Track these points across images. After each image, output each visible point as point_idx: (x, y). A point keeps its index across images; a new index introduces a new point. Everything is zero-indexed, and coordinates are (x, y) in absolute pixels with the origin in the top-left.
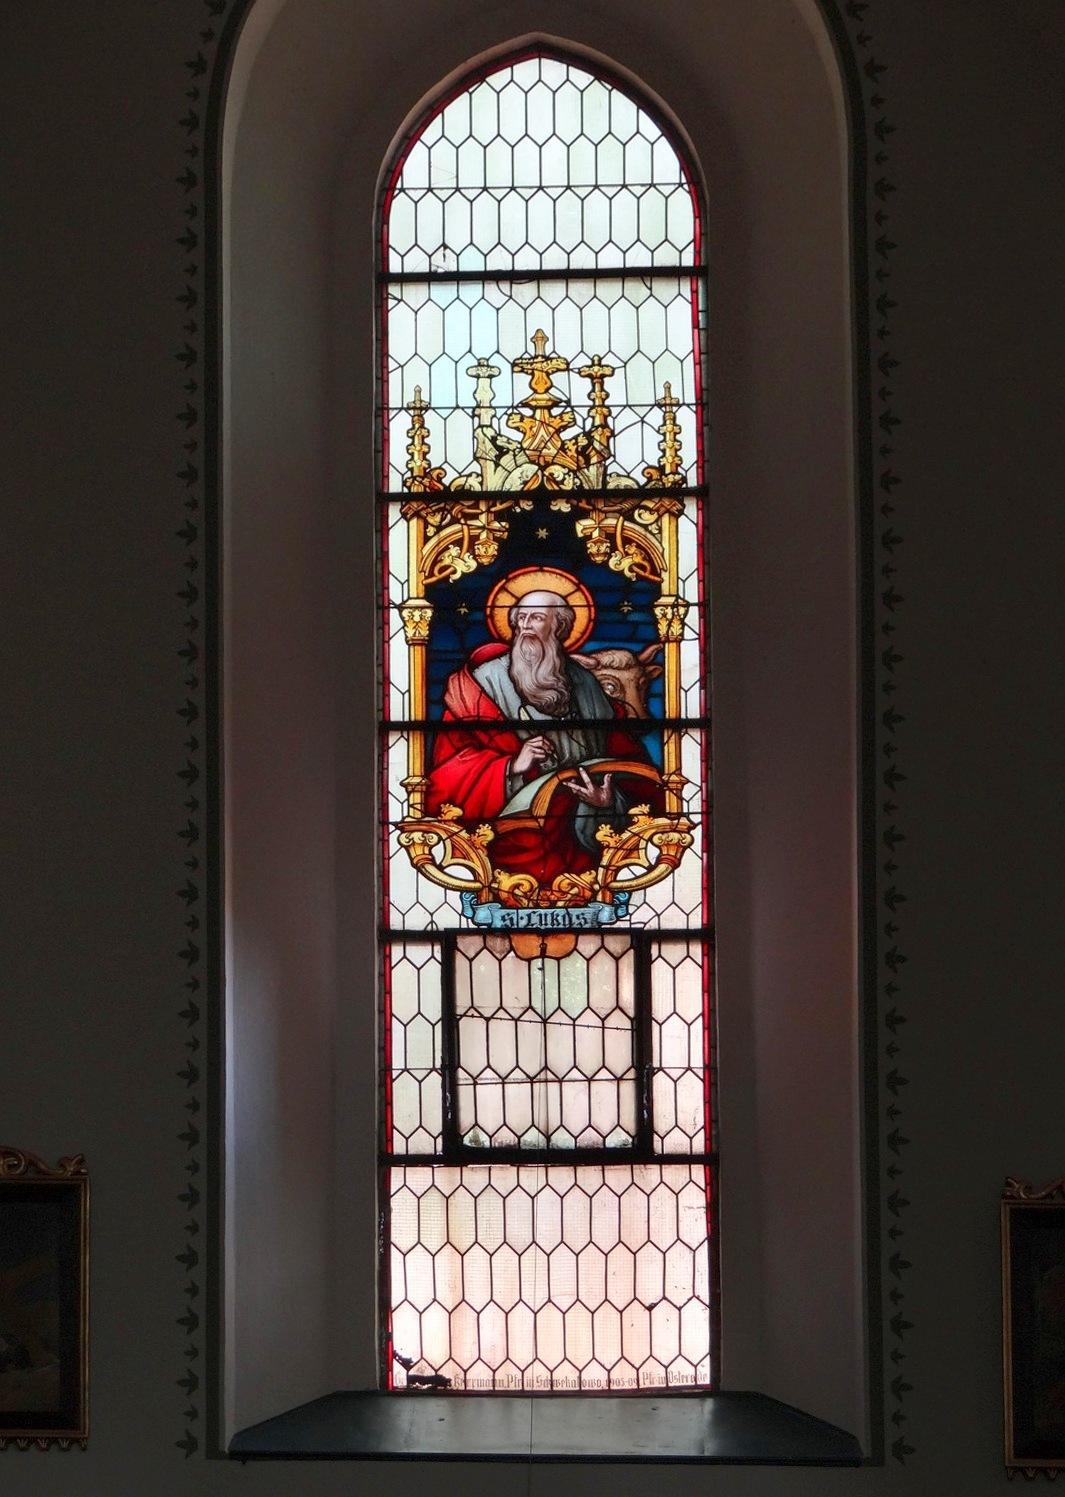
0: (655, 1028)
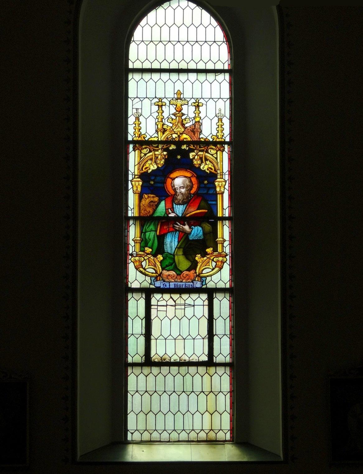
0: (214, 321)
